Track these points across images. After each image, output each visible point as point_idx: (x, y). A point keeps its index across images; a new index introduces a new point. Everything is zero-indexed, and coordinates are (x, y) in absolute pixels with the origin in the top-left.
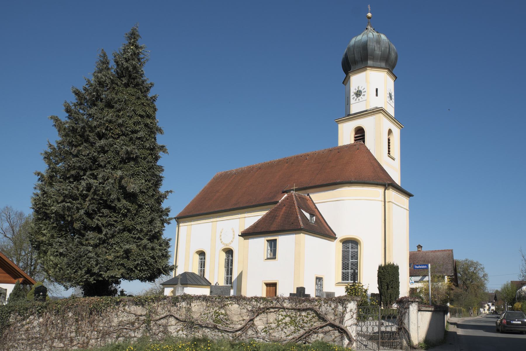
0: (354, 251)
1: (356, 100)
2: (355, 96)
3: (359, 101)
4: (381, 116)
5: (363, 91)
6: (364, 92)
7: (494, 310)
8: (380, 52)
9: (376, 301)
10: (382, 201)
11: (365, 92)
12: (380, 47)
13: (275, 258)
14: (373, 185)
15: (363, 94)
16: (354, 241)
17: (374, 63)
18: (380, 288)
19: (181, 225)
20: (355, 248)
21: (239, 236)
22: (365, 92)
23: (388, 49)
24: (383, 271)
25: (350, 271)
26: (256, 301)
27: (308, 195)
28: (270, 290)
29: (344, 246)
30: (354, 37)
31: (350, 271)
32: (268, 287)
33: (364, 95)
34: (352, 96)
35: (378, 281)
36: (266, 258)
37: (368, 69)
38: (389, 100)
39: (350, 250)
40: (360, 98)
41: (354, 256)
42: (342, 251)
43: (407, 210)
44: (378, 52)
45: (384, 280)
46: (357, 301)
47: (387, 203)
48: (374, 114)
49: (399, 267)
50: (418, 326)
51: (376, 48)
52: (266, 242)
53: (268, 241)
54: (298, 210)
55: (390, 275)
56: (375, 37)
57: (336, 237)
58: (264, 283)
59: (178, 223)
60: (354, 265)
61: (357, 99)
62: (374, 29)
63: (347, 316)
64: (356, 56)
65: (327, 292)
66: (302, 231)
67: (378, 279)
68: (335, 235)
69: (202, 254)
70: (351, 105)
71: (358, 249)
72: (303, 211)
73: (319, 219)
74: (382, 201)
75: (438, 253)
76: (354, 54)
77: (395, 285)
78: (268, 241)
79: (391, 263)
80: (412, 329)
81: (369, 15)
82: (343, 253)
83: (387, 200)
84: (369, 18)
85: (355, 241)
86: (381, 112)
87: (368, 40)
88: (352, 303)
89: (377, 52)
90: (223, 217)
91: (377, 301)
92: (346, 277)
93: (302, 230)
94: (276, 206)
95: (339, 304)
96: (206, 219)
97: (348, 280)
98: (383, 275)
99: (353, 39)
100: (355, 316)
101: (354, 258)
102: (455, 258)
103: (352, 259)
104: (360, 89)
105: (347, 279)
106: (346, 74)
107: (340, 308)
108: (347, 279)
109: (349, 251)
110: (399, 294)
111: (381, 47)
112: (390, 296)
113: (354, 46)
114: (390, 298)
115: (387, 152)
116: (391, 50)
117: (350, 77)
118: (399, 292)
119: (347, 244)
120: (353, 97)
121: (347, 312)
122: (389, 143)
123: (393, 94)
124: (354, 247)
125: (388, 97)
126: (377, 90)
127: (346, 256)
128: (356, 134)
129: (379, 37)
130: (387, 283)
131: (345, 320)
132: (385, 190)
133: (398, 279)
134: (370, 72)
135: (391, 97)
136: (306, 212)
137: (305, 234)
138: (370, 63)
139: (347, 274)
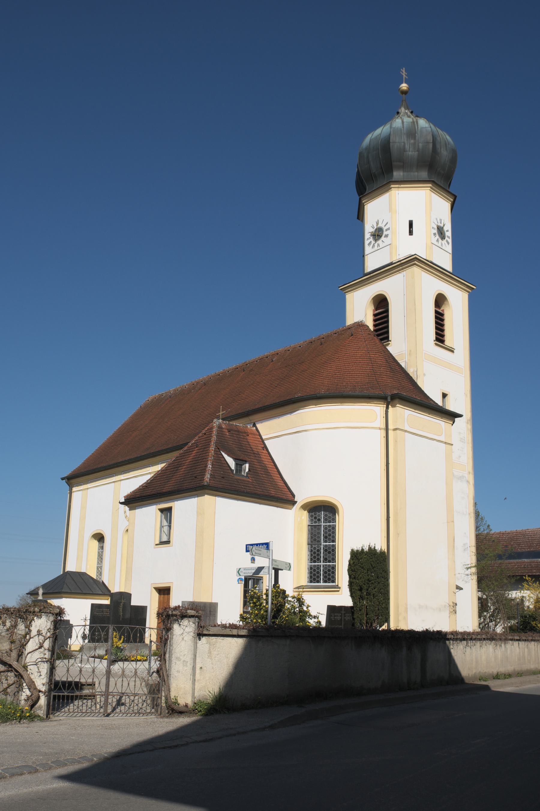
1: (373, 246)
2: (371, 239)
3: (379, 248)
4: (415, 271)
5: (385, 229)
6: (386, 230)
8: (416, 153)
10: (380, 429)
12: (414, 144)
13: (247, 545)
14: (363, 400)
15: (385, 233)
16: (329, 506)
17: (405, 174)
19: (74, 489)
21: (121, 503)
22: (388, 229)
23: (431, 146)
25: (322, 564)
27: (254, 425)
29: (312, 516)
30: (373, 131)
31: (322, 564)
32: (162, 596)
34: (368, 239)
36: (158, 542)
37: (392, 186)
38: (438, 241)
39: (323, 524)
40: (380, 242)
41: (330, 535)
44: (411, 153)
46: (53, 614)
47: (391, 433)
48: (403, 269)
51: (407, 147)
52: (159, 513)
56: (405, 126)
57: (295, 500)
58: (154, 588)
59: (71, 486)
60: (329, 553)
61: (376, 245)
62: (412, 112)
63: (31, 645)
66: (207, 491)
68: (294, 496)
69: (100, 538)
70: (366, 257)
74: (380, 429)
78: (162, 510)
80: (178, 672)
81: (404, 86)
83: (391, 427)
84: (404, 93)
85: (331, 507)
86: (415, 264)
87: (392, 133)
88: (44, 619)
89: (410, 153)
90: (129, 472)
92: (314, 575)
93: (203, 489)
95: (19, 619)
96: (106, 478)
97: (318, 582)
99: (369, 135)
100: (47, 644)
101: (329, 539)
103: (325, 542)
104: (380, 225)
105: (317, 579)
107: (21, 627)
108: (317, 579)
109: (321, 525)
113: (368, 149)
115: (433, 336)
116: (438, 146)
119: (318, 514)
120: (369, 241)
121: (32, 636)
123: (448, 228)
128: (376, 309)
129: (414, 124)
131: (26, 652)
132: (387, 408)
134: (397, 192)
136: (229, 455)
137: (216, 496)
138: (397, 174)
139: (317, 570)
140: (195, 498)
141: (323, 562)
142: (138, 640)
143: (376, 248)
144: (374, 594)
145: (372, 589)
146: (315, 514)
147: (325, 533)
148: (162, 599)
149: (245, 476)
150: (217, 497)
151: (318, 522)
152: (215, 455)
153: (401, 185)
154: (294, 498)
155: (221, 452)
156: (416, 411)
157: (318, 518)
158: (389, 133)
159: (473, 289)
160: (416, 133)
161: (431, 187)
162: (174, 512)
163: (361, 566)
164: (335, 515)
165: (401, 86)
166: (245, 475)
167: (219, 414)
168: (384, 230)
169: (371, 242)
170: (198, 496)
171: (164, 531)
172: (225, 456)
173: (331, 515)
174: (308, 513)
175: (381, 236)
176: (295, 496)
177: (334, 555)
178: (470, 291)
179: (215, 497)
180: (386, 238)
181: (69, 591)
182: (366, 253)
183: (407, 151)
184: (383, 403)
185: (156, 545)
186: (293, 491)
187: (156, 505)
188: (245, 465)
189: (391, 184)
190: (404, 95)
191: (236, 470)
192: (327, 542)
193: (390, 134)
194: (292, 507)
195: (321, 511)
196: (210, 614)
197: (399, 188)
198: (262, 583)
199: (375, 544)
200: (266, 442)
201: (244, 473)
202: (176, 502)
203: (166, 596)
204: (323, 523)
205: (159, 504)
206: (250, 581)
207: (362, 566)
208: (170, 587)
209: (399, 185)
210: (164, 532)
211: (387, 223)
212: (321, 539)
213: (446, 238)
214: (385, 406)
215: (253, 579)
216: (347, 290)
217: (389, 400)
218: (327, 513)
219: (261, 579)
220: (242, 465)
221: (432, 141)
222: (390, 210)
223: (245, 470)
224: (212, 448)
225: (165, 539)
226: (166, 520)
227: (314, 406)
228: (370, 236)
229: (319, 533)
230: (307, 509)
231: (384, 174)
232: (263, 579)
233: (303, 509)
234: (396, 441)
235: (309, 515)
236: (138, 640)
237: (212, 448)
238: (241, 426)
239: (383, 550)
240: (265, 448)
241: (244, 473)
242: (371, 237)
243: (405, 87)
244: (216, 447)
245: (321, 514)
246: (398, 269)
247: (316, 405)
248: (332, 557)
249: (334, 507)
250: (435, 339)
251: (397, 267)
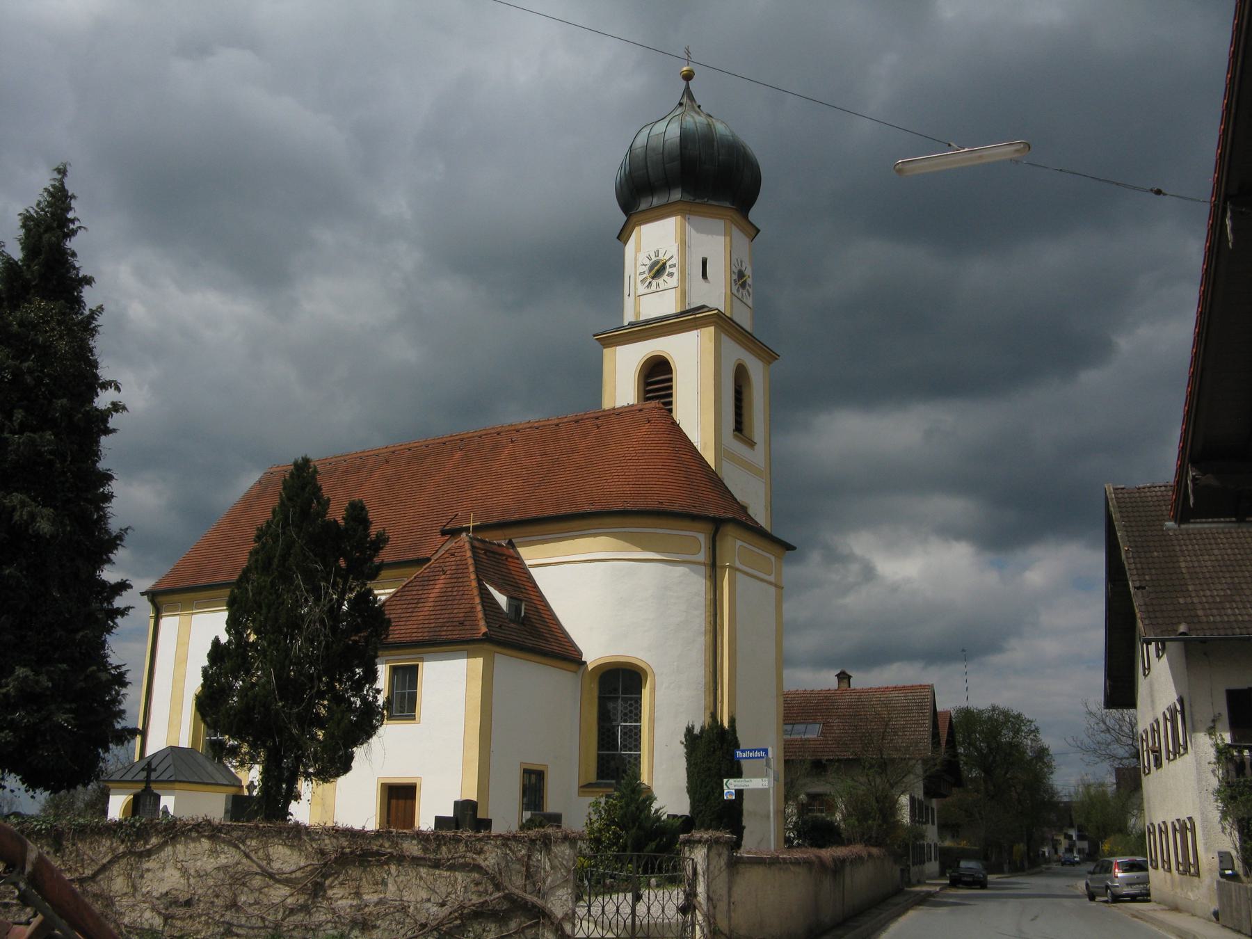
3: (658, 289)
7: (1086, 851)
26: (330, 836)
40: (660, 281)
41: (631, 711)
50: (729, 903)
54: (474, 584)
75: (893, 695)
94: (418, 571)
101: (631, 718)
102: (939, 709)
106: (626, 215)
120: (644, 276)
142: (650, 871)
143: (653, 288)
169: (646, 278)
172: (491, 589)
178: (1145, 645)
181: (213, 782)
204: (622, 694)
208: (416, 784)
236: (650, 871)
248: (634, 743)
249: (636, 670)
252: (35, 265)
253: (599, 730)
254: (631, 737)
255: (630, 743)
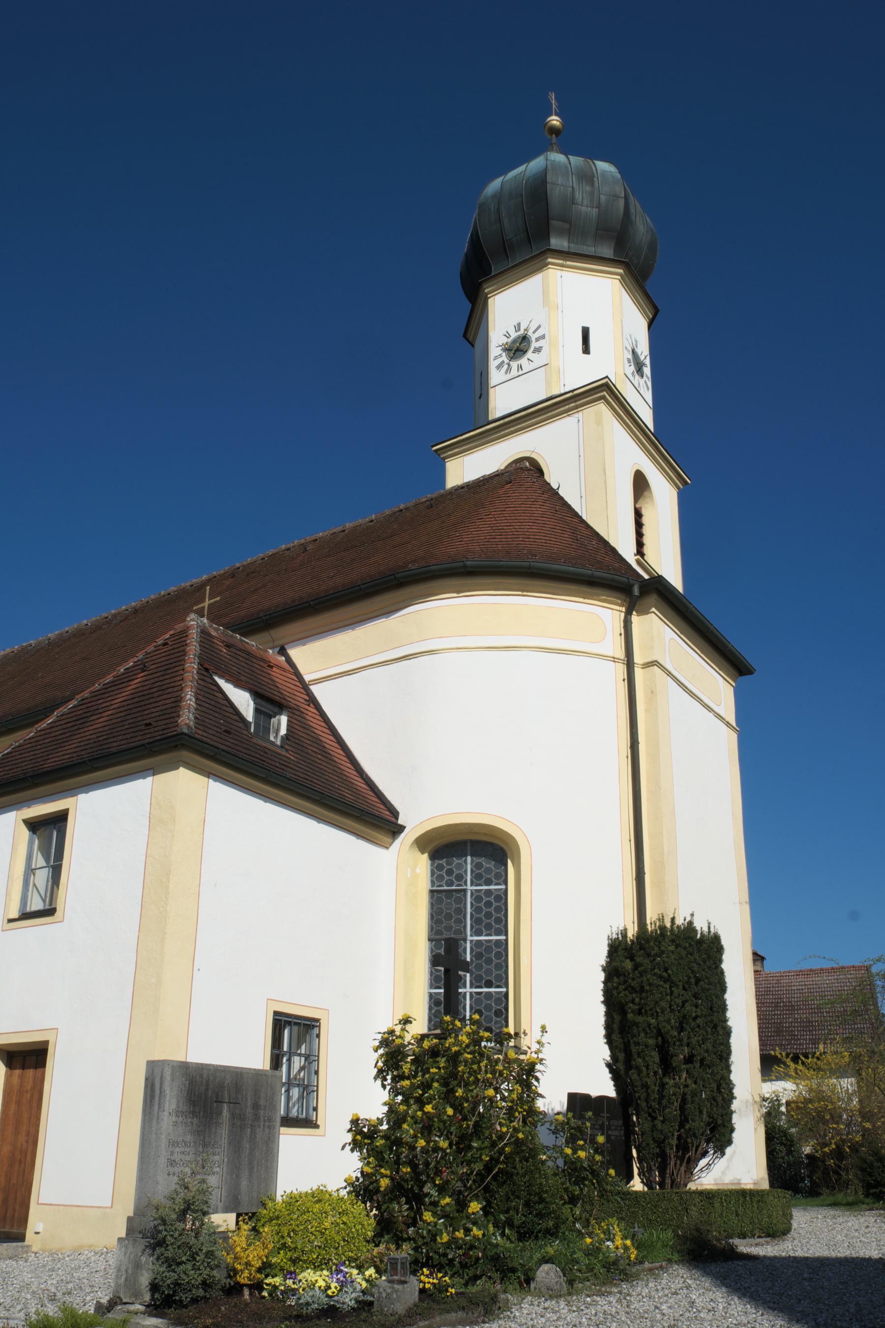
0: (488, 893)
1: (509, 369)
2: (504, 358)
3: (521, 372)
4: (601, 410)
5: (533, 337)
6: (537, 340)
8: (595, 211)
9: (593, 1141)
10: (614, 659)
11: (543, 337)
15: (534, 345)
18: (621, 1066)
20: (492, 876)
23: (622, 203)
24: (636, 967)
27: (283, 651)
28: (21, 1085)
29: (440, 867)
32: (17, 1072)
33: (538, 350)
34: (496, 358)
35: (608, 1026)
36: (15, 914)
37: (550, 260)
38: (633, 373)
39: (469, 887)
40: (523, 361)
42: (432, 892)
43: (728, 724)
44: (585, 208)
45: (640, 1019)
47: (638, 673)
49: (724, 942)
51: (578, 196)
52: (25, 833)
53: (27, 822)
55: (673, 984)
57: (400, 822)
64: (506, 222)
65: (201, 1068)
66: (185, 754)
67: (608, 1014)
68: (395, 814)
70: (491, 391)
71: (506, 882)
72: (221, 682)
73: (306, 727)
74: (614, 659)
76: (500, 220)
77: (708, 1045)
78: (34, 825)
79: (679, 921)
81: (555, 121)
82: (432, 905)
83: (638, 659)
84: (554, 131)
85: (492, 844)
86: (603, 398)
87: (549, 167)
91: (601, 1139)
93: (176, 747)
98: (633, 990)
103: (478, 933)
109: (465, 891)
110: (732, 1097)
111: (596, 192)
112: (682, 1108)
114: (681, 1125)
117: (486, 300)
118: (730, 1086)
119: (456, 861)
120: (499, 360)
122: (639, 525)
124: (488, 870)
125: (629, 360)
126: (585, 333)
127: (449, 917)
130: (659, 1033)
132: (628, 613)
133: (723, 1008)
135: (639, 370)
136: (238, 684)
137: (209, 774)
140: (144, 778)
141: (471, 987)
143: (514, 372)
144: (702, 1061)
145: (698, 1041)
146: (448, 864)
147: (477, 910)
148: (16, 1080)
149: (277, 746)
150: (211, 781)
151: (456, 883)
152: (200, 682)
153: (566, 261)
154: (397, 819)
155: (216, 678)
156: (682, 636)
157: (456, 872)
158: (545, 167)
159: (686, 482)
160: (594, 177)
161: (620, 275)
162: (75, 829)
163: (661, 977)
164: (506, 865)
165: (549, 119)
166: (279, 743)
167: (202, 605)
168: (533, 339)
170: (155, 771)
171: (34, 885)
173: (491, 865)
174: (430, 859)
175: (526, 351)
176: (398, 813)
177: (503, 966)
179: (206, 779)
180: (536, 354)
182: (493, 381)
183: (577, 204)
184: (620, 602)
185: (10, 921)
186: (393, 802)
187: (18, 809)
188: (277, 717)
189: (548, 255)
190: (554, 135)
191: (257, 725)
192: (480, 935)
193: (546, 169)
194: (390, 840)
195: (466, 856)
196: (256, 1117)
197: (563, 266)
198: (318, 1036)
199: (692, 915)
200: (313, 688)
201: (276, 737)
202: (82, 797)
203: (30, 1073)
205: (29, 807)
206: (286, 1032)
207: (665, 975)
208: (46, 1043)
209: (563, 260)
210: (35, 890)
211: (539, 327)
212: (465, 927)
213: (645, 377)
214: (624, 609)
215: (296, 1024)
216: (450, 453)
217: (636, 591)
218: (482, 860)
219: (314, 1026)
220: (270, 717)
221: (623, 195)
222: (546, 302)
223: (277, 731)
224: (192, 666)
225: (36, 904)
226: (43, 855)
227: (455, 595)
228: (501, 352)
229: (461, 911)
230: (430, 848)
231: (531, 244)
232: (319, 1026)
233: (418, 847)
234: (652, 692)
235: (432, 865)
237: (192, 666)
238: (253, 646)
239: (706, 929)
240: (313, 701)
241: (276, 737)
242: (504, 354)
243: (557, 120)
244: (201, 667)
245: (466, 864)
246: (567, 407)
247: (458, 592)
250: (636, 552)
251: (564, 404)
252: (304, 1076)
253: (432, 917)
254: (489, 961)
255: (489, 972)
